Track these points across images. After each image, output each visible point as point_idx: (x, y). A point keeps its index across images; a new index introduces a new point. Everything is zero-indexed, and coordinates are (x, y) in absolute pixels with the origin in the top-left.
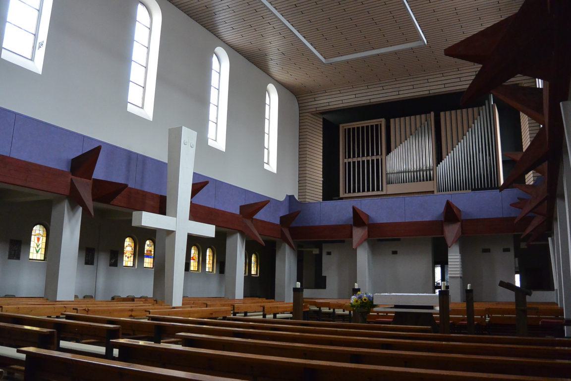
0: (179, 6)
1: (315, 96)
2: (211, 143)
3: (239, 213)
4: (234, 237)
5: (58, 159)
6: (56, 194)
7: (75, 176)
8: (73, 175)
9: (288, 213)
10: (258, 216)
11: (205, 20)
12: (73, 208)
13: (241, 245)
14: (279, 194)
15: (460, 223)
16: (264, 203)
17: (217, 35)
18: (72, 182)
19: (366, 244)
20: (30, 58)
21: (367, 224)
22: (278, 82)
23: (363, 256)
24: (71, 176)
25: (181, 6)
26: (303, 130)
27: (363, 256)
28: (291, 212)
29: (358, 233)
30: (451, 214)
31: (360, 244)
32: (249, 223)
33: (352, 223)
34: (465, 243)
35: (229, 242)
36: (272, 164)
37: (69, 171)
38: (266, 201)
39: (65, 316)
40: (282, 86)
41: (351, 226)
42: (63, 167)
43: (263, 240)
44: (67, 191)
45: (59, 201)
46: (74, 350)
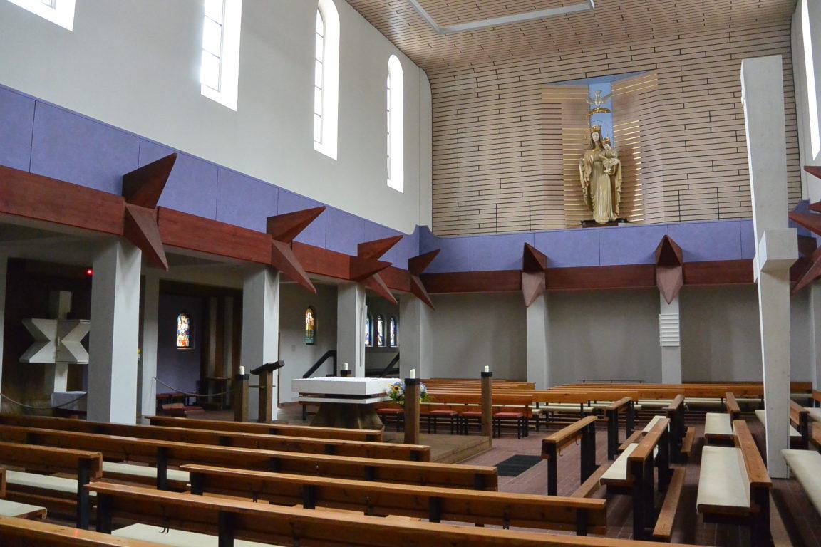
0: (357, 8)
1: (455, 74)
2: (317, 147)
3: (265, 232)
4: (257, 278)
5: (99, 173)
6: (22, 213)
7: (132, 203)
8: (127, 201)
9: (418, 255)
10: (301, 238)
11: (376, 20)
12: (127, 252)
13: (360, 302)
14: (404, 224)
15: (680, 268)
16: (394, 240)
17: (388, 36)
18: (127, 211)
19: (542, 299)
20: (217, 89)
21: (544, 268)
22: (404, 53)
23: (536, 318)
24: (125, 204)
25: (356, 5)
26: (437, 120)
27: (536, 318)
28: (425, 252)
29: (532, 284)
30: (668, 254)
31: (533, 300)
32: (283, 248)
33: (520, 267)
34: (686, 297)
35: (342, 301)
36: (396, 180)
37: (120, 194)
38: (396, 237)
39: (396, 417)
40: (410, 59)
41: (521, 272)
42: (112, 189)
43: (314, 284)
44: (118, 229)
45: (345, 287)
46: (61, 492)
